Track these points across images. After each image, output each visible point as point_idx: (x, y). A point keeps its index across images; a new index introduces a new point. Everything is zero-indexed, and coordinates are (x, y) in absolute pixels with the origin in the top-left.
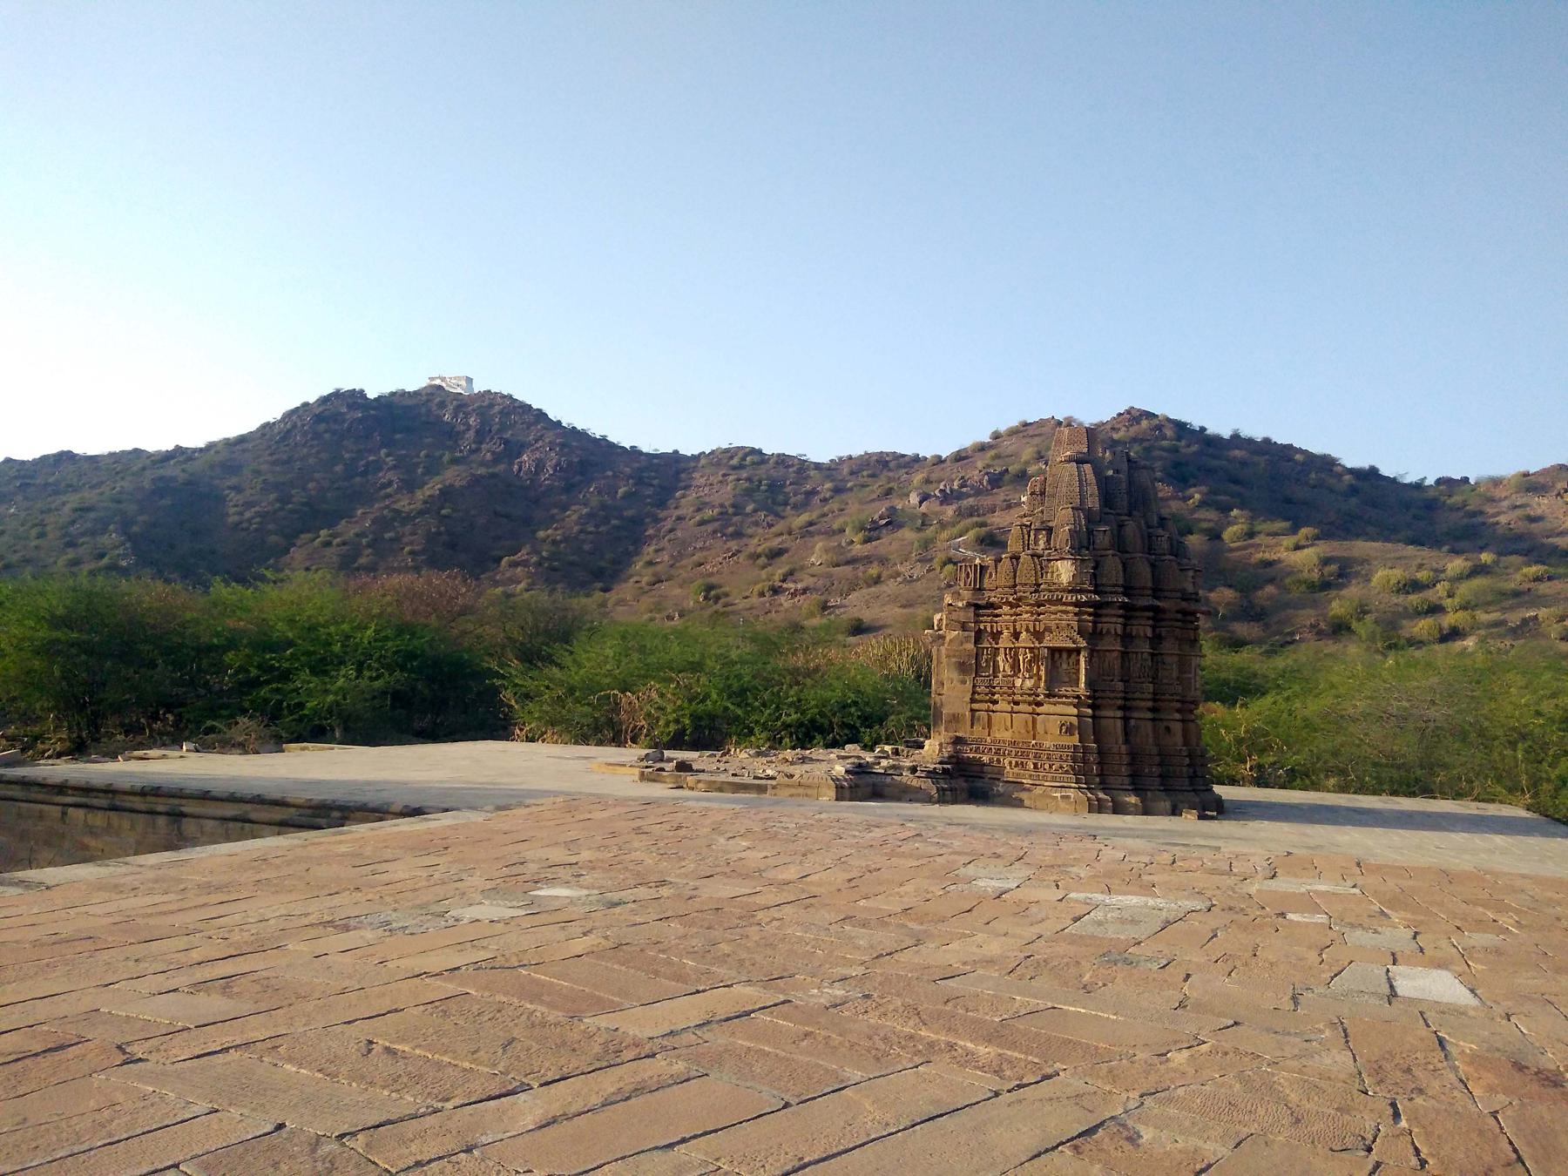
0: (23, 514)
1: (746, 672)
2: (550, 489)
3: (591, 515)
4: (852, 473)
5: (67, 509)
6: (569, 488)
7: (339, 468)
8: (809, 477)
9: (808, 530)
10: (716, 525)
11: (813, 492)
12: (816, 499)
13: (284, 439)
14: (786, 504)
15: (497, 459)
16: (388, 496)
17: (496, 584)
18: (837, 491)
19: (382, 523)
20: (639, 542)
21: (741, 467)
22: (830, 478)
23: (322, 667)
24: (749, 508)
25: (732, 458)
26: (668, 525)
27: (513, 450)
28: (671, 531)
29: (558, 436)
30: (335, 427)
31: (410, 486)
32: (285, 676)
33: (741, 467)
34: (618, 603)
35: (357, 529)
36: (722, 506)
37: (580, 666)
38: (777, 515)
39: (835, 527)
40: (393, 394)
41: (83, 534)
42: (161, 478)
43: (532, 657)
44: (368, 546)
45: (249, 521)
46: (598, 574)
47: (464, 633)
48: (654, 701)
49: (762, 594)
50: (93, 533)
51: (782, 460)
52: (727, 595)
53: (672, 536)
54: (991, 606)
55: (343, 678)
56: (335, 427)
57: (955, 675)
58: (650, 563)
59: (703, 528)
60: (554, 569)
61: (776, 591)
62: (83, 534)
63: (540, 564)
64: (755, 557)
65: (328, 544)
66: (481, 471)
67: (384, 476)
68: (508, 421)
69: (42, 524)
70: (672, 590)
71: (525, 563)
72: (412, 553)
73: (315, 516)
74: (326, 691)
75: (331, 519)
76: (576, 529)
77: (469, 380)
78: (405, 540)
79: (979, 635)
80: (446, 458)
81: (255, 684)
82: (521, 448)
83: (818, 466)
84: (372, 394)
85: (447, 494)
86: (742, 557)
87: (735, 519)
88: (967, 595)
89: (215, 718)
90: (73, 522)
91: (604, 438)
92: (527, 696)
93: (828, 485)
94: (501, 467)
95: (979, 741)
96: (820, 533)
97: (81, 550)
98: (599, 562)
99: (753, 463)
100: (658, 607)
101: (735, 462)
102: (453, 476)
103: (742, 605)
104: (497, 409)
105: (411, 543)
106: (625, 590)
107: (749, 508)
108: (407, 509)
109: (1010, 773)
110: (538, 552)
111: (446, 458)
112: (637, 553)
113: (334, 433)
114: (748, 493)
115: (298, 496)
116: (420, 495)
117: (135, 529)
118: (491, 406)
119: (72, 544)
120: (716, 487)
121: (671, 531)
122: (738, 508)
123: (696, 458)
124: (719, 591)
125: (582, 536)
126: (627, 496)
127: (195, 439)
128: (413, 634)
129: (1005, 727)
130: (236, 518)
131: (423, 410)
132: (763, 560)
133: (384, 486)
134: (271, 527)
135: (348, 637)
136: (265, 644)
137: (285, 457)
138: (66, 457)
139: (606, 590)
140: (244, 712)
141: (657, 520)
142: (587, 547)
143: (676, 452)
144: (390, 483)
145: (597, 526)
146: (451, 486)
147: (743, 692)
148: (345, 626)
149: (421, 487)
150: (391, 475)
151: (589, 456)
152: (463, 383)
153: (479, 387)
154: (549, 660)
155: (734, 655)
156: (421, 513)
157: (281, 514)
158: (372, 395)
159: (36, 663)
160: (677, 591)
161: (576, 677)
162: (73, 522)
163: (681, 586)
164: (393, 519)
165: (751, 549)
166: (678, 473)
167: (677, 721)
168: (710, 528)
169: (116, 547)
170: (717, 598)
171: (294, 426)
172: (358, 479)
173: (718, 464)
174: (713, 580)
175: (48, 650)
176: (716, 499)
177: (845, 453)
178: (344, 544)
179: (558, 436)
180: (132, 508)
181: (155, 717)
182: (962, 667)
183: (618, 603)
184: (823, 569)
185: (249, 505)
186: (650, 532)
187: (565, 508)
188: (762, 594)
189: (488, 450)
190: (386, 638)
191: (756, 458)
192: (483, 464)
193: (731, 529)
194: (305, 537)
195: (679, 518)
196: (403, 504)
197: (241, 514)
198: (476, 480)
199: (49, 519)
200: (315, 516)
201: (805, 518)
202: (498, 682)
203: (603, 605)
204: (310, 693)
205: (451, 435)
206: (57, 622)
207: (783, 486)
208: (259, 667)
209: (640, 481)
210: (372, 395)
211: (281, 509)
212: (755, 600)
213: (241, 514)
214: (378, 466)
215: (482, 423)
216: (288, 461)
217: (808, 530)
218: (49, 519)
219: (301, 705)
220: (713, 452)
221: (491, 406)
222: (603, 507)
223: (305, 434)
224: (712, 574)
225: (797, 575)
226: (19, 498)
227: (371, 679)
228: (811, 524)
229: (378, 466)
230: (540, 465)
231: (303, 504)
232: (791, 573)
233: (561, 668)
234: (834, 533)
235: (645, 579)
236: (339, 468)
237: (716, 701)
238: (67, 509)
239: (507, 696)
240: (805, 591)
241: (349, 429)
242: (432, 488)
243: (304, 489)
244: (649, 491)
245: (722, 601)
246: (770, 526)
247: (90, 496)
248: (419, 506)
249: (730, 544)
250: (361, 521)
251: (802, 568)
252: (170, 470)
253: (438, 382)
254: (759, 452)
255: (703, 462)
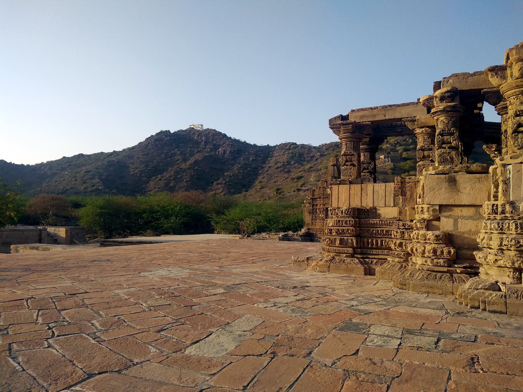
0: (70, 174)
1: (271, 215)
2: (229, 159)
3: (241, 167)
4: (326, 149)
5: (83, 172)
6: (234, 159)
7: (163, 155)
8: (312, 151)
9: (310, 170)
10: (282, 168)
11: (313, 157)
12: (315, 159)
13: (146, 147)
14: (304, 161)
15: (211, 150)
16: (178, 164)
17: (212, 190)
18: (322, 155)
19: (177, 173)
20: (257, 175)
21: (289, 149)
22: (319, 151)
23: (167, 217)
24: (292, 163)
25: (286, 146)
26: (266, 169)
27: (216, 147)
28: (267, 171)
29: (230, 142)
30: (161, 142)
31: (185, 160)
32: (158, 219)
33: (289, 149)
34: (250, 195)
35: (169, 174)
36: (283, 162)
37: (230, 214)
38: (302, 164)
39: (319, 168)
40: (179, 131)
41: (88, 179)
42: (110, 161)
43: (219, 213)
44: (173, 180)
45: (137, 173)
46: (244, 186)
47: (202, 207)
48: (248, 223)
49: (294, 191)
50: (91, 179)
51: (303, 146)
52: (283, 192)
53: (267, 173)
54: (315, 199)
55: (173, 219)
56: (161, 142)
57: (308, 214)
58: (261, 182)
59: (277, 170)
60: (229, 185)
61: (299, 190)
62: (88, 179)
63: (226, 184)
64: (293, 179)
65: (161, 180)
66: (207, 154)
67: (177, 158)
68: (214, 138)
69: (76, 177)
70: (266, 191)
71: (221, 183)
72: (186, 181)
73: (156, 171)
74: (168, 223)
75: (161, 172)
76: (237, 172)
77: (202, 125)
78: (184, 178)
79: (313, 205)
80: (196, 151)
81: (150, 222)
82: (219, 146)
83: (315, 148)
84: (172, 132)
85: (196, 162)
86: (289, 180)
87: (288, 166)
88: (311, 196)
89: (142, 230)
90: (84, 176)
91: (245, 142)
92: (217, 223)
93: (319, 154)
94: (213, 153)
95: (313, 229)
96: (314, 170)
97: (87, 184)
98: (243, 183)
99: (293, 148)
100: (262, 196)
101: (287, 147)
102: (198, 157)
103: (288, 194)
104: (211, 134)
105: (186, 178)
106: (252, 191)
107: (292, 163)
108: (184, 168)
109: (319, 235)
110: (225, 180)
111: (196, 151)
112: (256, 179)
113: (161, 145)
114: (292, 158)
115: (151, 165)
116: (188, 163)
117: (103, 177)
118: (209, 133)
119: (85, 183)
120: (281, 156)
121: (267, 171)
122: (289, 163)
123: (275, 147)
124: (281, 191)
125: (239, 174)
126: (253, 160)
127: (119, 149)
128: (189, 208)
129: (318, 225)
130: (132, 173)
131: (188, 136)
132: (295, 180)
133: (177, 161)
134: (143, 175)
135: (173, 209)
136: (152, 212)
137: (146, 153)
138: (81, 156)
139: (246, 191)
140: (148, 229)
141: (262, 168)
142: (240, 177)
143: (268, 145)
144: (179, 159)
145: (243, 171)
146: (198, 160)
147: (270, 220)
148: (172, 207)
149: (188, 160)
150: (179, 157)
151: (240, 148)
152: (200, 126)
153: (205, 127)
154: (223, 213)
155: (269, 211)
156: (189, 169)
157: (146, 171)
158: (172, 132)
159: (97, 218)
160: (268, 191)
161: (228, 218)
162: (84, 176)
163: (269, 189)
164: (180, 171)
165: (292, 177)
166: (269, 152)
167: (253, 228)
168: (280, 170)
169: (98, 183)
170: (280, 193)
171: (149, 143)
172: (169, 159)
173: (282, 149)
174: (280, 187)
175: (100, 215)
176: (281, 160)
177: (324, 143)
178: (165, 179)
179: (230, 142)
180: (102, 171)
181: (124, 231)
182: (310, 213)
183: (250, 195)
184: (314, 182)
185: (136, 168)
186: (260, 172)
187: (233, 165)
188: (294, 191)
189: (209, 147)
190: (182, 209)
191: (294, 146)
192: (207, 152)
193: (286, 170)
194: (154, 178)
195: (269, 167)
196: (183, 166)
197: (134, 171)
198: (205, 158)
199: (78, 175)
200: (156, 171)
201: (309, 165)
202: (210, 220)
203: (245, 196)
204: (164, 224)
205: (197, 143)
206: (101, 208)
207: (304, 155)
208: (151, 217)
209: (257, 156)
210: (172, 132)
211: (146, 169)
212: (292, 193)
213: (134, 171)
214: (175, 154)
215: (206, 139)
216: (148, 154)
217: (310, 170)
218: (78, 175)
219: (162, 227)
220: (280, 145)
221: (209, 133)
222: (245, 164)
223: (152, 145)
224: (279, 185)
225: (306, 185)
226: (68, 169)
227: (179, 220)
228: (311, 168)
229: (175, 154)
230: (225, 152)
231: (153, 167)
232: (304, 184)
233: (225, 215)
234: (319, 170)
235: (258, 187)
236: (163, 155)
237: (263, 223)
238: (83, 172)
239: (213, 223)
240: (308, 190)
241: (165, 143)
242: (191, 161)
243: (153, 163)
244: (260, 158)
245: (282, 194)
246: (299, 168)
247: (89, 167)
248: (188, 166)
249: (285, 175)
250: (170, 173)
251: (308, 182)
252: (113, 159)
253: (192, 126)
254: (295, 144)
255: (277, 148)
